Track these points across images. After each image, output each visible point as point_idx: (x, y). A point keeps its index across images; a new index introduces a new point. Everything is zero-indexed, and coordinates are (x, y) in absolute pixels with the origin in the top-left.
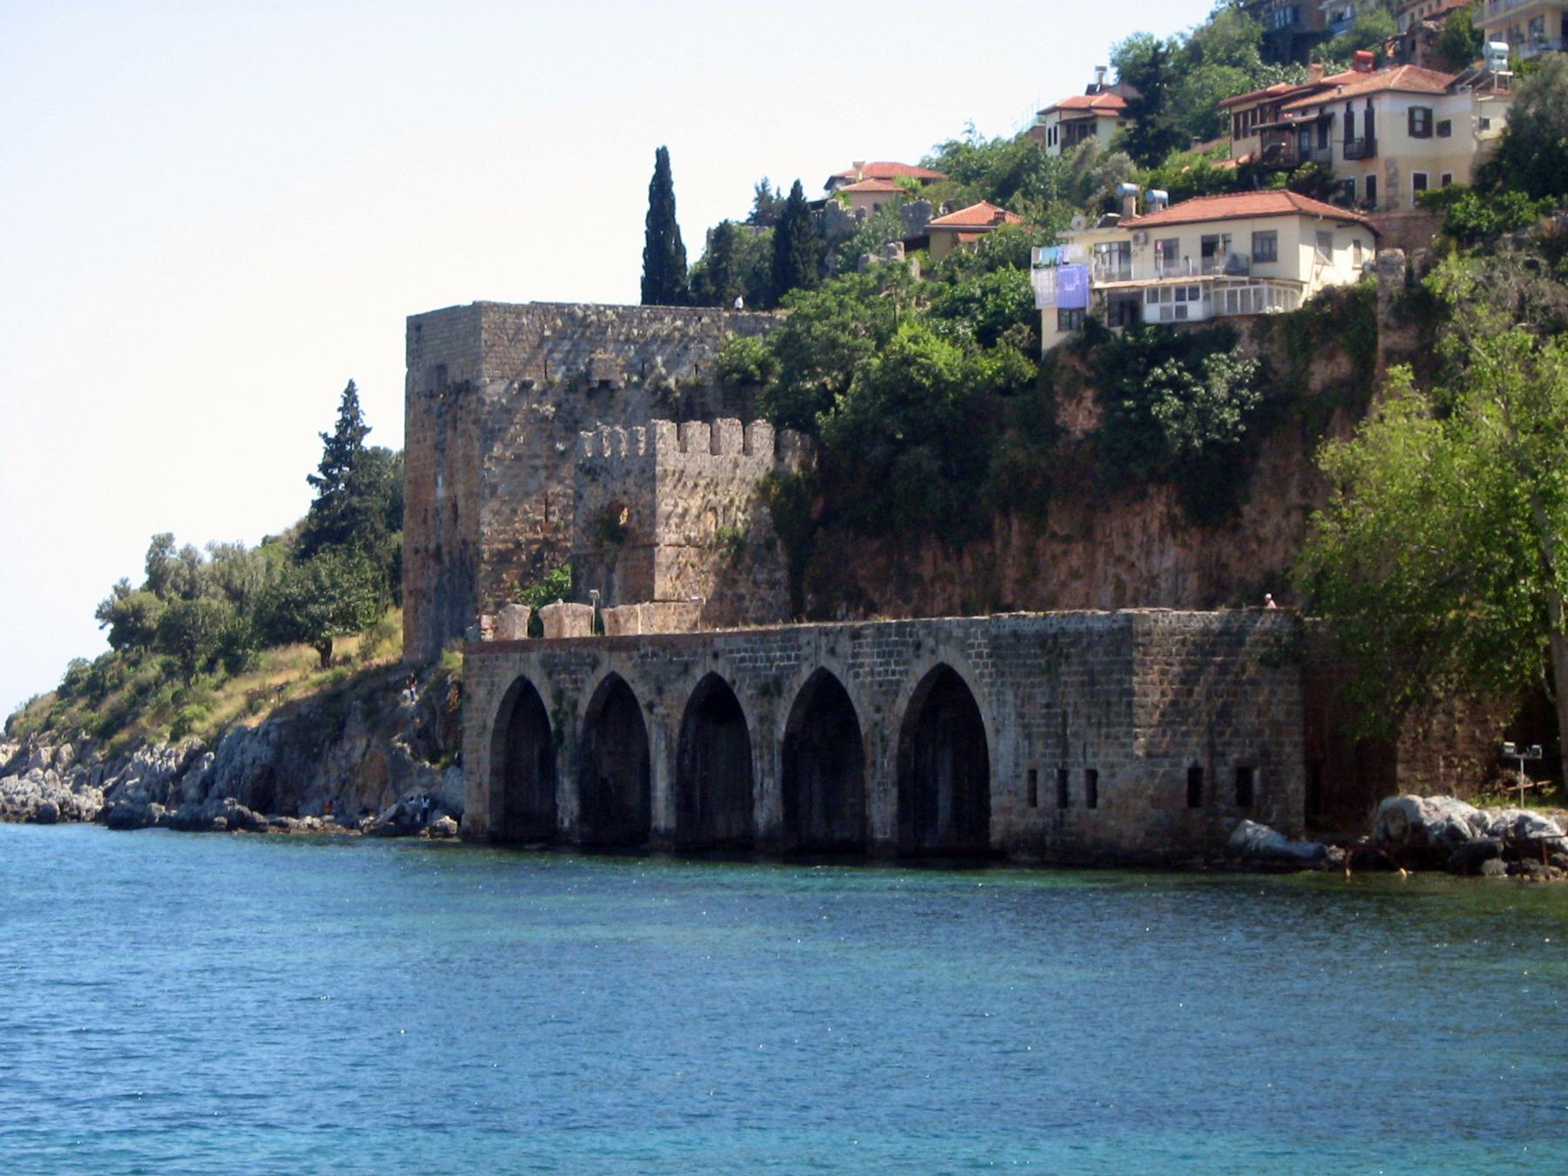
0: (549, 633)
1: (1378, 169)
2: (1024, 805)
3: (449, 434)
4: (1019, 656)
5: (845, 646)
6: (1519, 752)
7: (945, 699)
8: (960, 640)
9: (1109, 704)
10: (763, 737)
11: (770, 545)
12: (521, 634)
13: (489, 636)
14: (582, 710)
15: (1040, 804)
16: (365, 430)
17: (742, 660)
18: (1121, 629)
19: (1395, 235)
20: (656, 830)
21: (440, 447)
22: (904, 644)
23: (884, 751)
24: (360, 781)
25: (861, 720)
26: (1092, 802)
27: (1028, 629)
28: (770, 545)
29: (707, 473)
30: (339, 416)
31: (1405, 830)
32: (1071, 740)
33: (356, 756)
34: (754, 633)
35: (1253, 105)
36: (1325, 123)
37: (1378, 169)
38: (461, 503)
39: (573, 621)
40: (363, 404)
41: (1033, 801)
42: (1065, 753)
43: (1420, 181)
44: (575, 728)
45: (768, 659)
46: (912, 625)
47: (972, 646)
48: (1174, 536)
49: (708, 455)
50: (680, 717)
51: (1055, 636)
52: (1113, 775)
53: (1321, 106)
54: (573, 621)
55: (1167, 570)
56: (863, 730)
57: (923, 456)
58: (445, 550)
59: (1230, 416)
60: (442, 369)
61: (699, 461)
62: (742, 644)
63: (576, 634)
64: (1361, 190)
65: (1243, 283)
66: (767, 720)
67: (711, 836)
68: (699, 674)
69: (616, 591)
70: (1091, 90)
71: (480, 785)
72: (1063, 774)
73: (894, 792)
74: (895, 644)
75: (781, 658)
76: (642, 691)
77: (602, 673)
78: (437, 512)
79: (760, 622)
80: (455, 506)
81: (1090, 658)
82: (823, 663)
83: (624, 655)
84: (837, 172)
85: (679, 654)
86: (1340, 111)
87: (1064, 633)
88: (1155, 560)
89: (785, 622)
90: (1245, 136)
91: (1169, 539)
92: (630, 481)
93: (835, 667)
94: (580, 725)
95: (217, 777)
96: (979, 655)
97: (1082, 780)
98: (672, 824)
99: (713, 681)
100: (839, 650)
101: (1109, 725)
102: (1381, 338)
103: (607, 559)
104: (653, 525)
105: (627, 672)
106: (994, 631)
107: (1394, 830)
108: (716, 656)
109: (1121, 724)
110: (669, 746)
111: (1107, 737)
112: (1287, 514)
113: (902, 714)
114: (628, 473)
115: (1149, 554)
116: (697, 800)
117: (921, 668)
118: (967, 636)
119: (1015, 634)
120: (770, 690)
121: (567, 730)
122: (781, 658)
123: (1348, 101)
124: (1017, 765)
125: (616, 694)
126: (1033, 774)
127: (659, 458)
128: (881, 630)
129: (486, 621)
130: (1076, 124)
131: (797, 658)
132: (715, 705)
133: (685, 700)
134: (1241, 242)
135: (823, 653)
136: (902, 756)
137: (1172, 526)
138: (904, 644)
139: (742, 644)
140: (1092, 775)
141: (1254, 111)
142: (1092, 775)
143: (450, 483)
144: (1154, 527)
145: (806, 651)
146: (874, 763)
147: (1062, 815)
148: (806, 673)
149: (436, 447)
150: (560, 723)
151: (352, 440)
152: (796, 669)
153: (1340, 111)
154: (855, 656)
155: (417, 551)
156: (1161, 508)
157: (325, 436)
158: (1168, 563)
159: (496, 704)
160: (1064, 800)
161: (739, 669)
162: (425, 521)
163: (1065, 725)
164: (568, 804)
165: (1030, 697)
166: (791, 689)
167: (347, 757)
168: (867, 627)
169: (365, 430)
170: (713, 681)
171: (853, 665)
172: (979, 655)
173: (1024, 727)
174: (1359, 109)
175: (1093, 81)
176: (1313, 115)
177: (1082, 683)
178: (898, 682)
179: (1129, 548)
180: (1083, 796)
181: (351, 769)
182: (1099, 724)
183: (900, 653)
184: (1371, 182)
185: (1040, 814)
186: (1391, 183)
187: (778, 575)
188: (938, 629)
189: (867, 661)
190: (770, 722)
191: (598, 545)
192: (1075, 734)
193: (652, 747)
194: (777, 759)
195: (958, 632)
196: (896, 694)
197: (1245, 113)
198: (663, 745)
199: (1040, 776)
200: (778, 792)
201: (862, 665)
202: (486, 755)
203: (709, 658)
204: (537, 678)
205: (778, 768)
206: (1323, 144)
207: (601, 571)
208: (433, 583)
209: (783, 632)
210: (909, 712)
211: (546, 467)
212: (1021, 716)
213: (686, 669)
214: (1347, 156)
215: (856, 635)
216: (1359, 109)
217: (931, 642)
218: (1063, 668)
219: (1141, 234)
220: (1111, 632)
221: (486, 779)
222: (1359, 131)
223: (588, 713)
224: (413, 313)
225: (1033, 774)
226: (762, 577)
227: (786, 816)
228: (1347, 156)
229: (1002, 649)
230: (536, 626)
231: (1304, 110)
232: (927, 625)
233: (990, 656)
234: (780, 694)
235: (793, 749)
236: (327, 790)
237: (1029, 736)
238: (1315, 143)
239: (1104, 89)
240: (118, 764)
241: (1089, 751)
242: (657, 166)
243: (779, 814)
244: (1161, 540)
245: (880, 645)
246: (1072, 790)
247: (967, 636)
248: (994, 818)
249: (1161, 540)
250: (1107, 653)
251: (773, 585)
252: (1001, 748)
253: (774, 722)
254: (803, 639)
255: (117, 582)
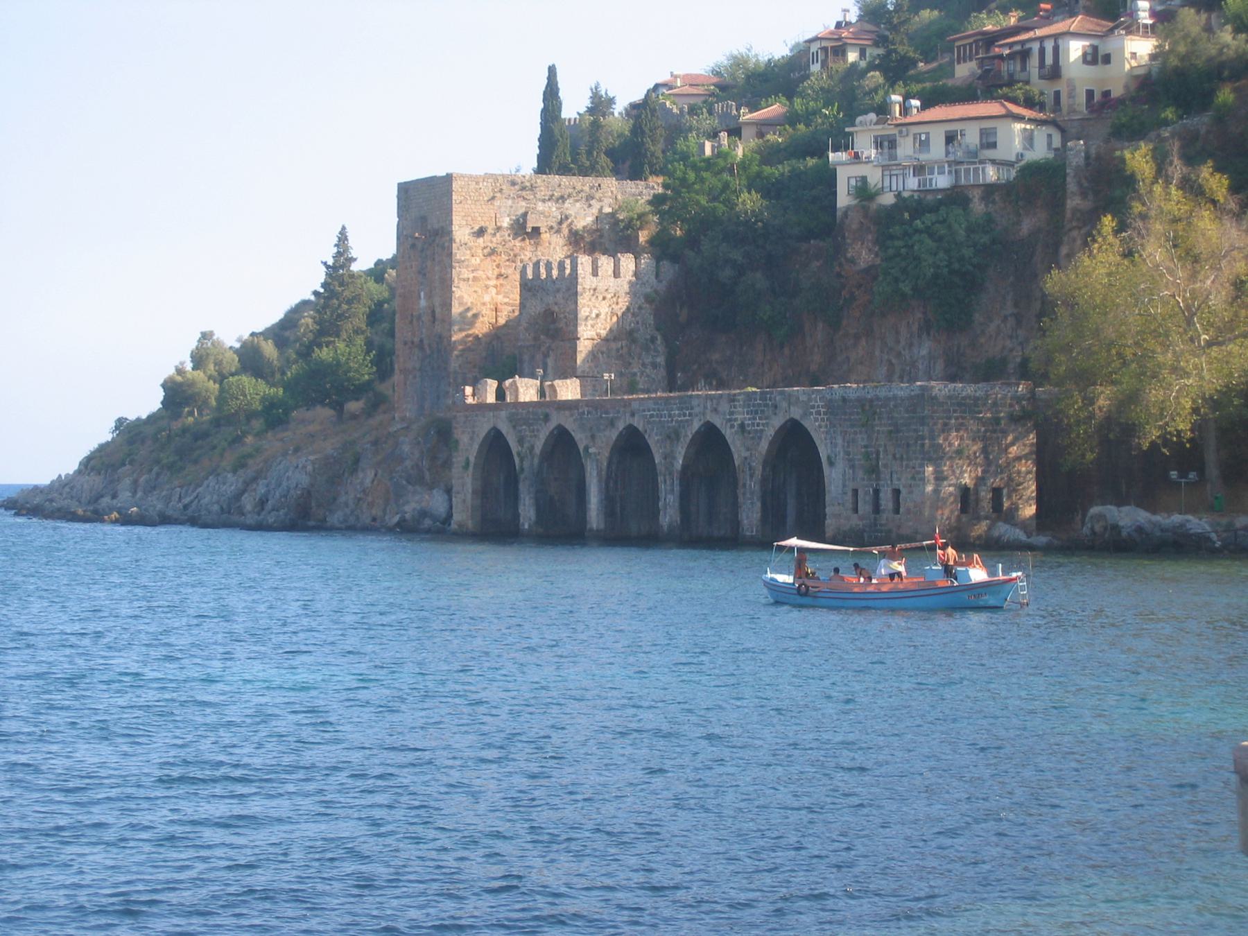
0: (509, 399)
1: (1062, 86)
2: (850, 512)
3: (429, 263)
4: (845, 414)
5: (724, 407)
6: (1181, 477)
7: (794, 445)
8: (804, 402)
9: (908, 445)
10: (667, 468)
11: (653, 340)
12: (491, 398)
13: (470, 400)
14: (538, 450)
15: (860, 512)
16: (353, 260)
17: (652, 416)
18: (918, 396)
19: (1074, 131)
20: (591, 530)
21: (422, 272)
22: (766, 405)
23: (752, 476)
24: (370, 499)
25: (736, 456)
26: (897, 510)
27: (852, 396)
28: (653, 340)
29: (612, 290)
30: (335, 250)
31: (1106, 528)
32: (882, 469)
33: (368, 481)
34: (660, 398)
35: (971, 40)
36: (1025, 55)
37: (1062, 86)
38: (438, 310)
39: (527, 390)
40: (351, 242)
41: (856, 510)
42: (878, 479)
43: (1090, 94)
44: (532, 464)
45: (670, 416)
46: (771, 393)
47: (813, 407)
48: (928, 334)
49: (612, 279)
50: (607, 455)
51: (871, 401)
52: (911, 492)
53: (1023, 43)
54: (527, 390)
55: (923, 357)
56: (737, 463)
57: (759, 279)
58: (426, 342)
59: (967, 252)
60: (423, 219)
61: (606, 279)
62: (651, 404)
63: (527, 400)
64: (1049, 100)
65: (974, 163)
66: (669, 457)
67: (630, 530)
68: (621, 426)
69: (550, 370)
70: (838, 25)
71: (464, 501)
72: (877, 492)
73: (759, 504)
74: (759, 405)
75: (679, 415)
76: (580, 438)
77: (552, 424)
78: (419, 318)
79: (647, 391)
80: (433, 312)
81: (896, 415)
82: (708, 418)
83: (567, 413)
84: (660, 81)
85: (607, 413)
86: (1036, 47)
87: (878, 399)
88: (915, 350)
89: (664, 391)
90: (965, 61)
91: (924, 336)
92: (559, 296)
93: (717, 421)
94: (536, 461)
95: (270, 497)
96: (819, 413)
97: (890, 495)
98: (602, 526)
99: (632, 431)
100: (720, 409)
101: (908, 459)
102: (1069, 201)
103: (543, 349)
104: (576, 326)
105: (570, 426)
106: (828, 397)
107: (1098, 528)
108: (633, 415)
109: (916, 459)
110: (599, 474)
111: (907, 466)
112: (1005, 319)
113: (764, 452)
114: (558, 290)
115: (911, 345)
116: (618, 510)
117: (777, 422)
118: (810, 400)
119: (844, 400)
120: (673, 436)
121: (526, 464)
122: (679, 415)
123: (1041, 39)
124: (844, 486)
125: (562, 441)
126: (855, 492)
127: (580, 280)
128: (748, 394)
129: (468, 390)
130: (833, 46)
131: (690, 415)
132: (632, 446)
133: (611, 443)
134: (972, 137)
135: (708, 411)
136: (764, 480)
137: (926, 327)
138: (766, 405)
139: (651, 404)
140: (897, 492)
141: (970, 45)
142: (897, 492)
143: (429, 297)
144: (915, 328)
145: (697, 410)
146: (744, 485)
147: (875, 519)
148: (696, 425)
149: (419, 272)
150: (522, 460)
151: (342, 267)
152: (689, 423)
153: (1036, 47)
154: (732, 413)
155: (405, 343)
156: (919, 315)
157: (325, 263)
158: (924, 352)
159: (476, 447)
160: (877, 509)
161: (649, 422)
162: (411, 322)
163: (878, 459)
164: (527, 513)
165: (854, 441)
166: (686, 436)
167: (362, 483)
168: (740, 394)
169: (353, 260)
170: (632, 431)
171: (730, 420)
172: (819, 413)
173: (850, 460)
174: (1049, 45)
175: (841, 19)
176: (1018, 48)
177: (891, 432)
178: (762, 431)
179: (898, 342)
180: (890, 506)
181: (364, 491)
182: (902, 458)
183: (763, 411)
184: (1057, 94)
185: (861, 518)
186: (1071, 95)
187: (658, 360)
188: (790, 395)
189: (739, 417)
190: (670, 457)
191: (536, 339)
192: (885, 466)
193: (588, 475)
194: (676, 482)
195: (803, 398)
196: (760, 438)
197: (964, 46)
198: (595, 473)
199: (860, 493)
200: (677, 504)
201: (736, 420)
202: (469, 480)
203: (628, 415)
204: (505, 428)
205: (677, 489)
206: (1024, 68)
207: (539, 357)
208: (417, 366)
209: (679, 397)
210: (769, 451)
211: (496, 287)
212: (848, 454)
213: (612, 423)
214: (1041, 77)
215: (732, 399)
216: (1049, 45)
217: (785, 404)
218: (877, 422)
219: (904, 129)
220: (911, 398)
221: (469, 496)
222: (1049, 60)
223: (542, 452)
224: (403, 181)
225: (855, 492)
226: (648, 360)
227: (682, 521)
228: (1041, 77)
229: (835, 409)
230: (500, 394)
231: (1011, 45)
232: (782, 393)
233: (825, 413)
234: (678, 439)
235: (687, 477)
236: (347, 505)
237: (853, 467)
238: (1018, 68)
239: (848, 24)
240: (191, 488)
241: (895, 476)
242: (549, 78)
243: (678, 519)
244: (919, 336)
245: (749, 406)
246: (883, 502)
247: (810, 400)
248: (828, 522)
249: (919, 336)
250: (907, 411)
251: (655, 365)
252: (834, 475)
253: (674, 458)
254: (695, 402)
255: (177, 363)
